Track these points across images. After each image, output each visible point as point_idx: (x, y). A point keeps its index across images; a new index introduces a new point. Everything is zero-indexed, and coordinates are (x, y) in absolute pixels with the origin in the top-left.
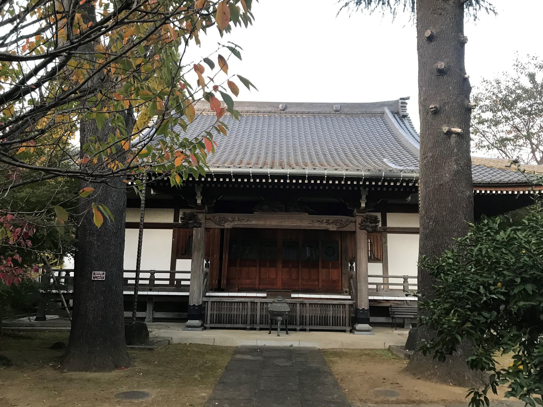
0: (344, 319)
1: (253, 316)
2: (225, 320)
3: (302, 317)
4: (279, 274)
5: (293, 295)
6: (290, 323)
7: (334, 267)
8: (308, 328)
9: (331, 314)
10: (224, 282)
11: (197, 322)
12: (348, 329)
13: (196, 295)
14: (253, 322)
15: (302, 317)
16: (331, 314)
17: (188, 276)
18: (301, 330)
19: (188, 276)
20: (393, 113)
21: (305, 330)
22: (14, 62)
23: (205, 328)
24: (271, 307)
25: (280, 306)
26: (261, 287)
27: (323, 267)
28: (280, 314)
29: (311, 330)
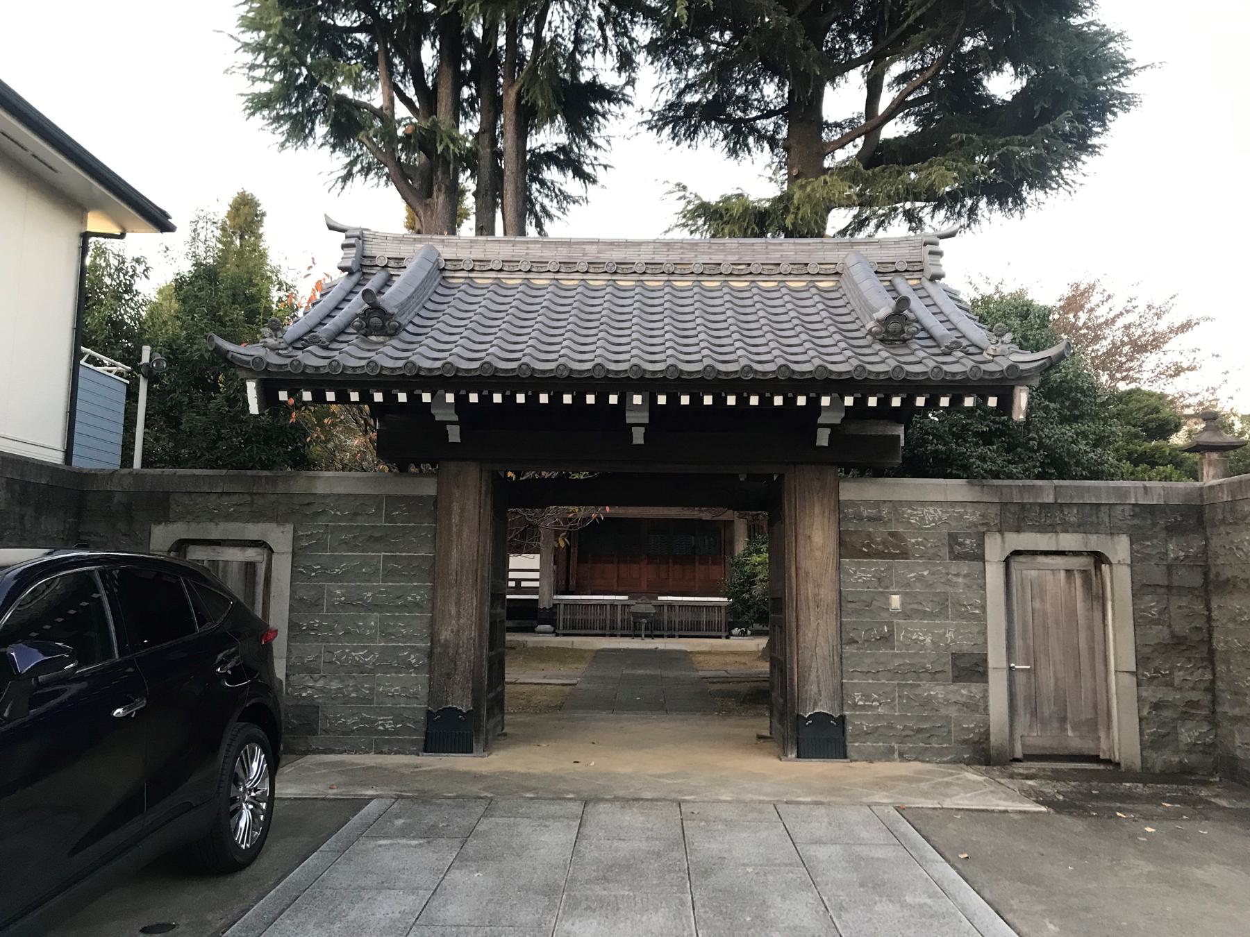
0: (720, 623)
1: (613, 621)
2: (582, 623)
3: (670, 622)
4: (645, 573)
5: (660, 598)
6: (655, 628)
7: (714, 563)
8: (676, 634)
9: (704, 618)
10: (572, 582)
11: (548, 627)
12: (724, 634)
13: (547, 597)
14: (612, 628)
15: (670, 622)
16: (704, 618)
17: (536, 575)
18: (669, 636)
19: (536, 575)
20: (433, 744)
21: (673, 636)
22: (768, 664)
23: (557, 635)
24: (633, 609)
25: (643, 607)
26: (621, 589)
27: (701, 563)
28: (645, 616)
29: (680, 636)
